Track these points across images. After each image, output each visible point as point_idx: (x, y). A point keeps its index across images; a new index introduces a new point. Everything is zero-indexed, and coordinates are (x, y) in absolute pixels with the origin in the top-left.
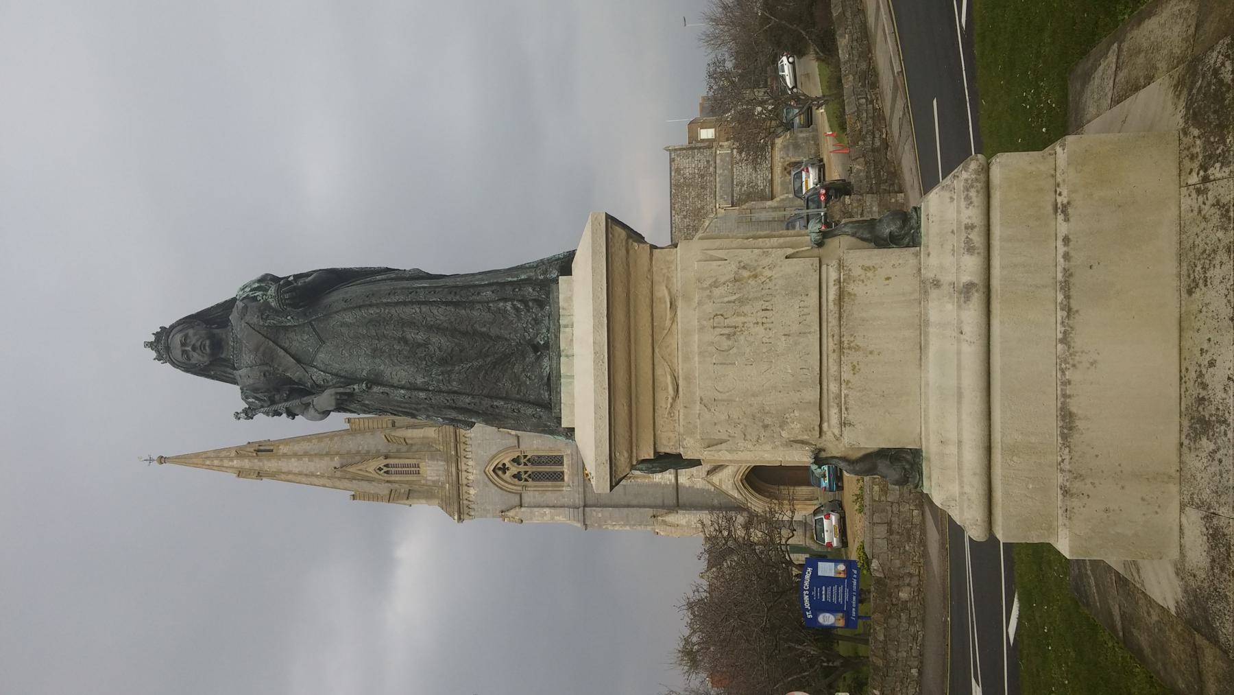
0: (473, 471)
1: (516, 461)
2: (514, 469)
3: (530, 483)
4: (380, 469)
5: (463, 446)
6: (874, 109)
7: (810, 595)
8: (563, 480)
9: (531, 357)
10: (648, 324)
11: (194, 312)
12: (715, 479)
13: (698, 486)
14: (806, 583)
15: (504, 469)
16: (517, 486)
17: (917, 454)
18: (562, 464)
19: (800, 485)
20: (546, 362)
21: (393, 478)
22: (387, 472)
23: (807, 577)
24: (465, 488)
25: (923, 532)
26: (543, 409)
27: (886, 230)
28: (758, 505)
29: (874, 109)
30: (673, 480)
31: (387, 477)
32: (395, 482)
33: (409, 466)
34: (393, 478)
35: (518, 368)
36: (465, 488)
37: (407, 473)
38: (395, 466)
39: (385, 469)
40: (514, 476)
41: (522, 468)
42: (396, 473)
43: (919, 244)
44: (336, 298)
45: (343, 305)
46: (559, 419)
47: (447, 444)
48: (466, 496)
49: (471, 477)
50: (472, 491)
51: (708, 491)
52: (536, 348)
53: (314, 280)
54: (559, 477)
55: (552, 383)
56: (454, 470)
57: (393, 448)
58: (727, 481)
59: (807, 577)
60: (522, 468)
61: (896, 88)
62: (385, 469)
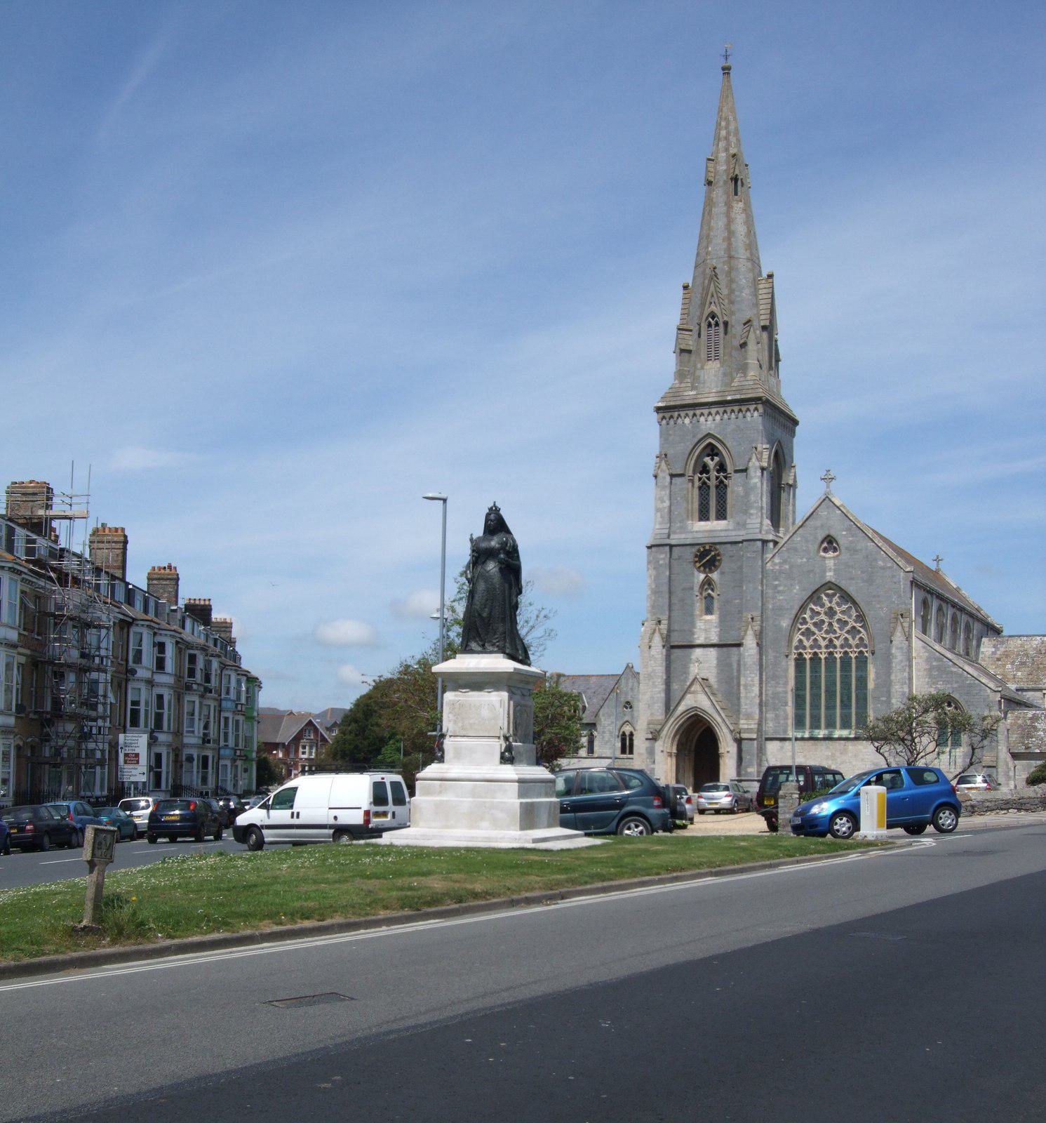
0: (709, 423)
1: (722, 467)
5: (736, 408)
8: (701, 520)
17: (443, 762)
31: (704, 325)
36: (691, 413)
43: (501, 763)
48: (683, 414)
49: (702, 419)
50: (687, 421)
52: (483, 645)
54: (704, 516)
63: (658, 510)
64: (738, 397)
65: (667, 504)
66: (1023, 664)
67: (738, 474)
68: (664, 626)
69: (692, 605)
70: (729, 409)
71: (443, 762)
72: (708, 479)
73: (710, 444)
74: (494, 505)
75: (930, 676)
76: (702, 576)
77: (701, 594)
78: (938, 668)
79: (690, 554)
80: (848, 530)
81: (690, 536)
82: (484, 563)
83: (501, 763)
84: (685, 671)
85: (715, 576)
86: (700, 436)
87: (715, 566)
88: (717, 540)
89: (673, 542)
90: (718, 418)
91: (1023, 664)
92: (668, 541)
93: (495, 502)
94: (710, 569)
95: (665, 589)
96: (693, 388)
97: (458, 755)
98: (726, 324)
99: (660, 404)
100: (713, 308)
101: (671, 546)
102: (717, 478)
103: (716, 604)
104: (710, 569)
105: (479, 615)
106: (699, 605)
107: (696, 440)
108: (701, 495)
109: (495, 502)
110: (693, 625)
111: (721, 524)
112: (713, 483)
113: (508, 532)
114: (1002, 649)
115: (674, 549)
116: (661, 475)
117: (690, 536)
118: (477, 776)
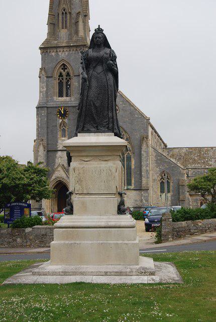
0: (63, 55)
1: (68, 74)
2: (64, 73)
3: (58, 81)
4: (64, 10)
5: (75, 49)
6: (206, 230)
7: (16, 206)
8: (59, 97)
9: (95, 125)
10: (100, 155)
11: (107, 38)
12: (60, 169)
13: (57, 160)
14: (21, 204)
15: (64, 69)
16: (56, 75)
17: (72, 214)
18: (67, 96)
19: (58, 207)
20: (93, 129)
21: (60, 16)
22: (63, 13)
23: (24, 204)
24: (55, 50)
25: (43, 247)
26: (82, 127)
27: (122, 207)
28: (50, 186)
29: (206, 230)
30: (59, 149)
31: (60, 13)
32: (58, 18)
33: (66, 24)
34: (60, 16)
35: (92, 122)
36: (55, 50)
37: (63, 23)
38: (66, 17)
39: (64, 12)
40: (61, 74)
41: (65, 77)
42: (63, 17)
43: (118, 213)
44: (110, 76)
45: (108, 79)
46: (79, 133)
47: (77, 41)
48: (52, 51)
49: (60, 53)
50: (53, 54)
51: (54, 165)
52: (97, 127)
53: (115, 70)
54: (61, 95)
55: (89, 131)
56: (64, 45)
57: (74, 15)
58: (59, 174)
59: (24, 204)
60: (65, 77)
61: (211, 237)
62: (64, 12)
63: (40, 92)
64: (75, 44)
65: (45, 89)
66: (180, 159)
67: (76, 77)
68: (45, 142)
69: (57, 133)
70: (72, 49)
71: (72, 214)
72: (63, 79)
73: (63, 64)
74: (99, 27)
75: (157, 163)
76: (61, 121)
77: (60, 128)
78: (160, 160)
79: (55, 111)
80: (123, 102)
81: (55, 103)
82: (94, 67)
83: (118, 213)
84: (54, 162)
85: (66, 120)
86: (59, 61)
87: (66, 117)
88: (67, 105)
89: (48, 106)
90: (67, 53)
91: (180, 159)
92: (46, 105)
93: (99, 26)
94: (64, 118)
95: (45, 126)
96: (55, 40)
97: (85, 209)
98: (70, 13)
99: (42, 46)
100: (64, 6)
101: (47, 107)
102: (66, 79)
103: (67, 133)
104: (64, 118)
105: (94, 104)
106: (60, 134)
107: (57, 62)
108: (59, 86)
109: (99, 26)
110: (57, 142)
111: (68, 99)
112: (64, 81)
113: (109, 47)
114: (171, 153)
115: (49, 109)
116: (42, 77)
117: (55, 103)
118: (103, 224)
